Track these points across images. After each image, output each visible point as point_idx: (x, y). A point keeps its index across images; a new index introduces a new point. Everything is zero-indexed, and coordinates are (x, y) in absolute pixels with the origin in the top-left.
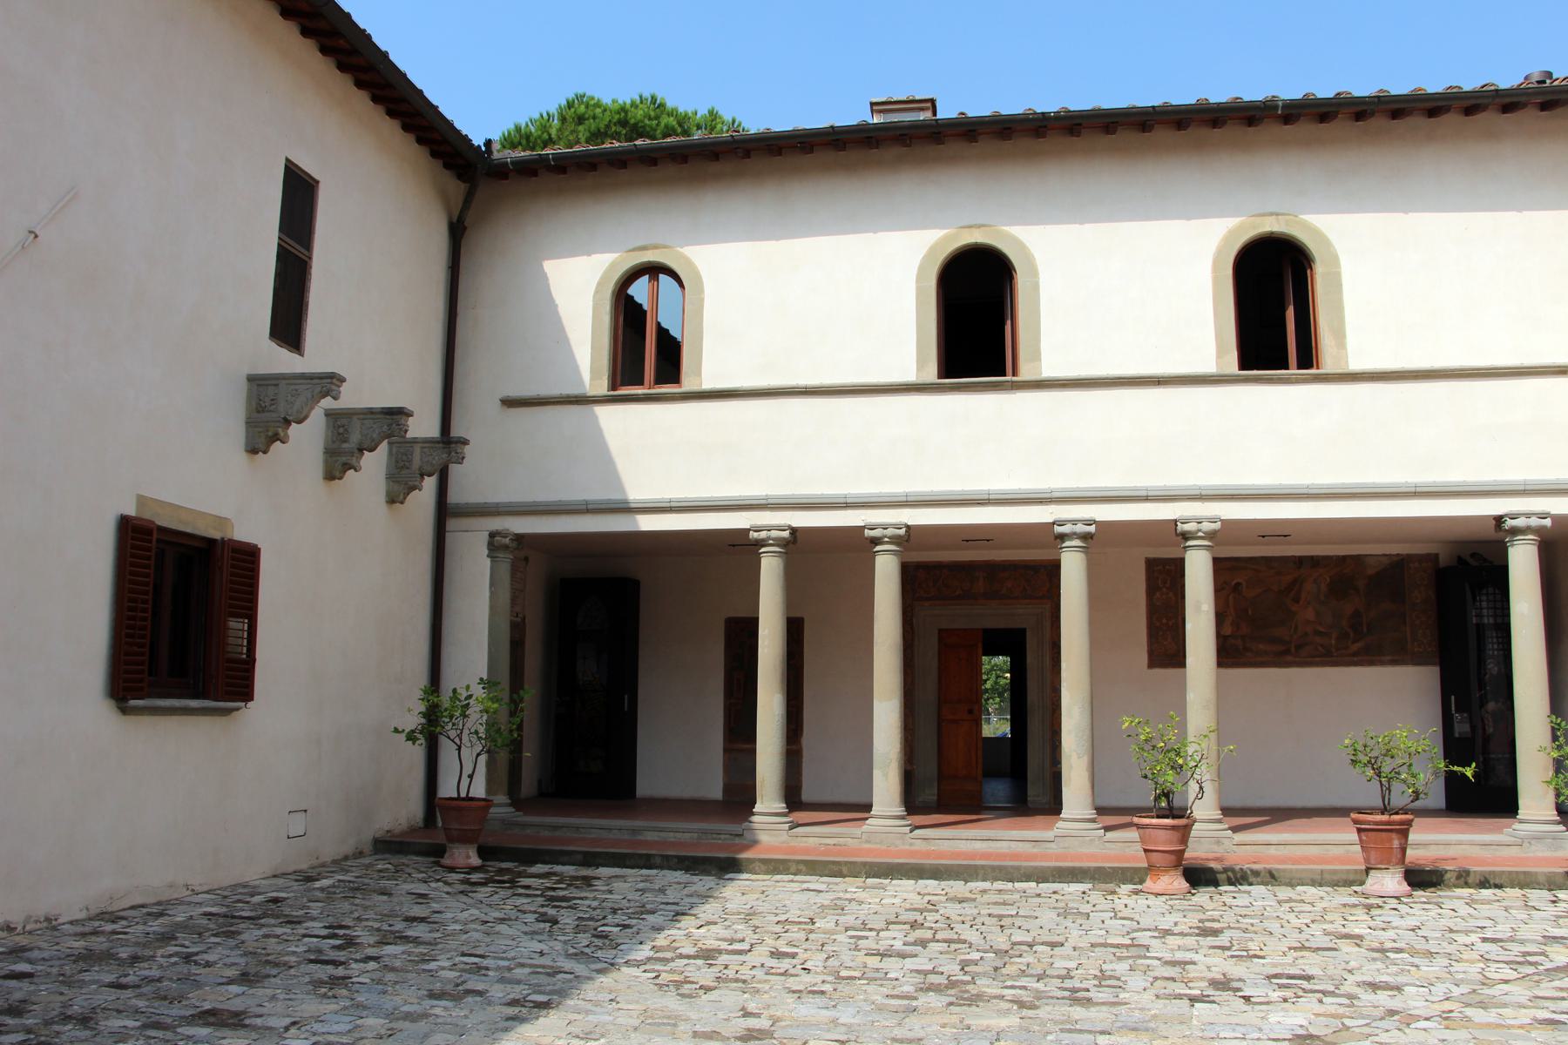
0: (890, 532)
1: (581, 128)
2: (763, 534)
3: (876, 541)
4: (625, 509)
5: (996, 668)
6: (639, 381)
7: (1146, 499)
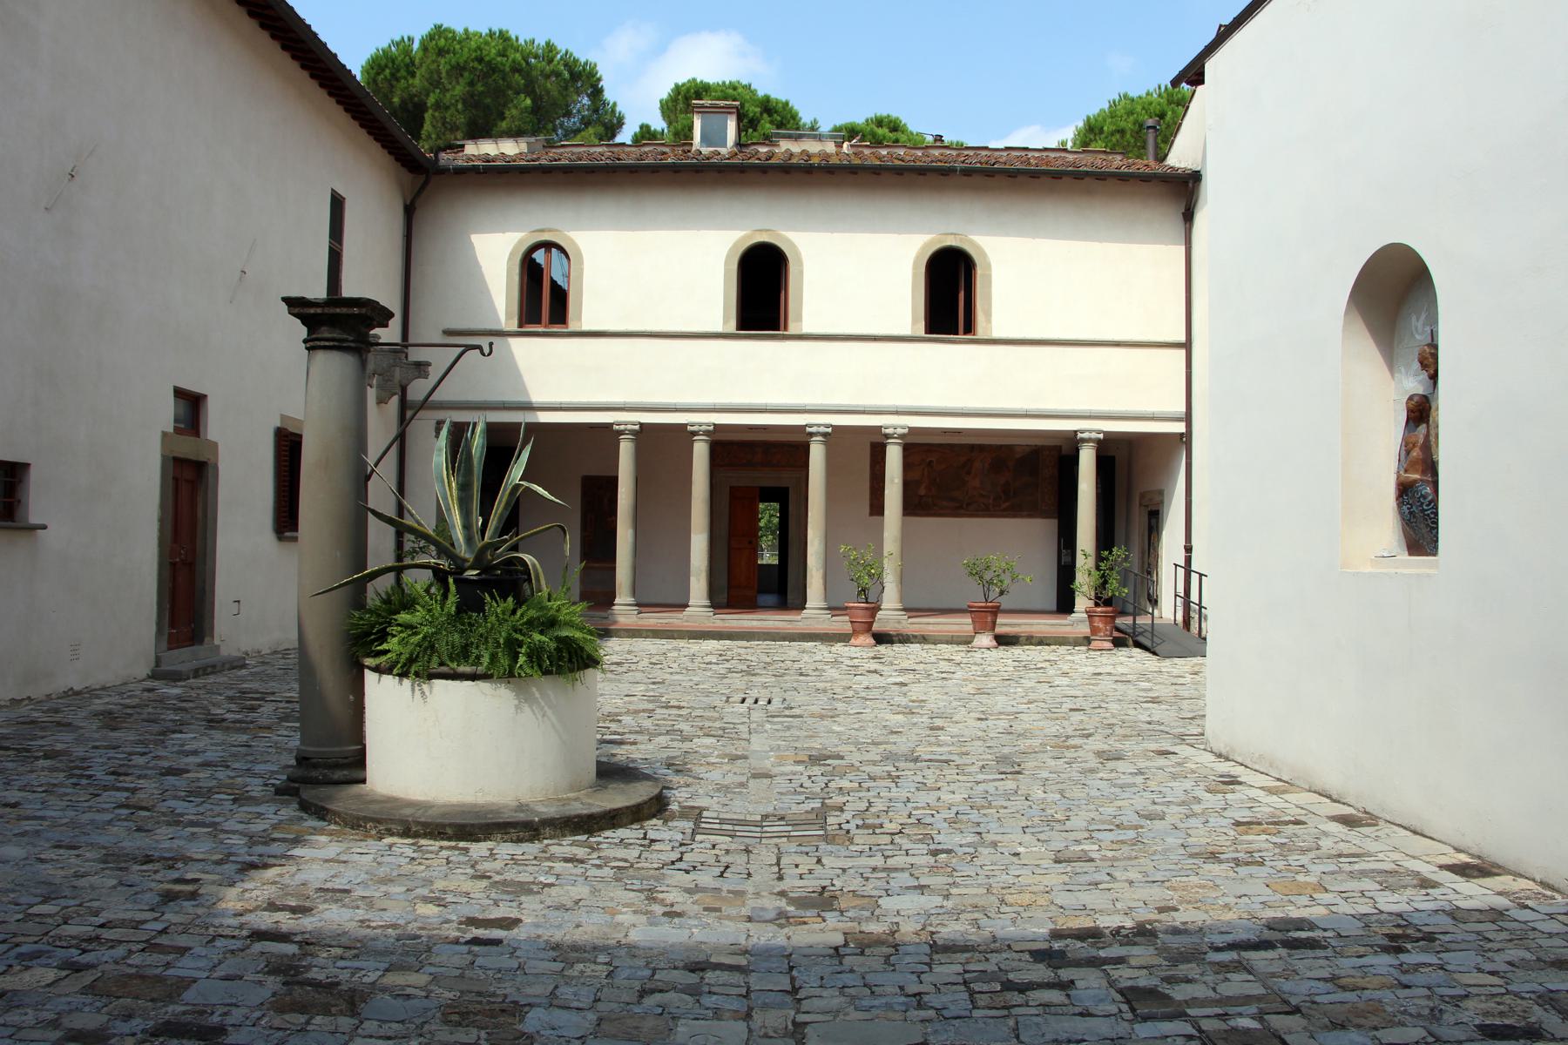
0: (704, 428)
1: (443, 61)
2: (622, 427)
3: (694, 433)
4: (530, 407)
5: (768, 514)
6: (538, 321)
7: (864, 412)
